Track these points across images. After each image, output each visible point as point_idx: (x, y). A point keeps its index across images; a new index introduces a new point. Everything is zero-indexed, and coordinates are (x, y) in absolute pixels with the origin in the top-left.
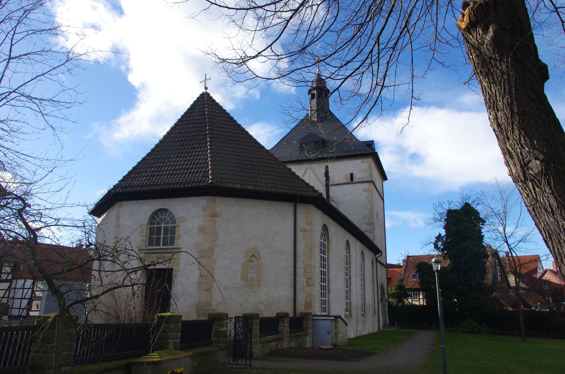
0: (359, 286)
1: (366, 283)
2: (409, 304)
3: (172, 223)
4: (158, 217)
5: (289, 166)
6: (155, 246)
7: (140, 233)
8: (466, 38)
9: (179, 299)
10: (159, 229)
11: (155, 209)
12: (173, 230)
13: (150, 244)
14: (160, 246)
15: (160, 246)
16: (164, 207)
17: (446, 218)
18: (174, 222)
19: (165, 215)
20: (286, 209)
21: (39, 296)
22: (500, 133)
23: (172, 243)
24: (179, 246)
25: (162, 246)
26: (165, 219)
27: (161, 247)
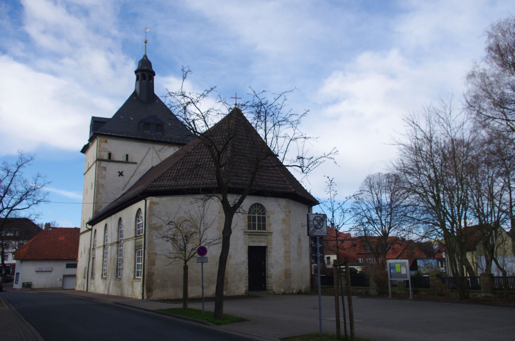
0: (345, 303)
1: (343, 321)
2: (380, 236)
3: (263, 214)
4: (253, 209)
5: (287, 167)
6: (253, 230)
7: (243, 220)
8: (379, 201)
9: (273, 267)
10: (254, 217)
11: (256, 202)
12: (264, 219)
13: (249, 228)
14: (256, 230)
15: (256, 230)
16: (259, 202)
17: (407, 239)
18: (264, 214)
19: (258, 208)
20: (93, 202)
21: (376, 212)
22: (393, 190)
23: (264, 228)
24: (271, 231)
25: (258, 230)
26: (258, 211)
27: (257, 231)
